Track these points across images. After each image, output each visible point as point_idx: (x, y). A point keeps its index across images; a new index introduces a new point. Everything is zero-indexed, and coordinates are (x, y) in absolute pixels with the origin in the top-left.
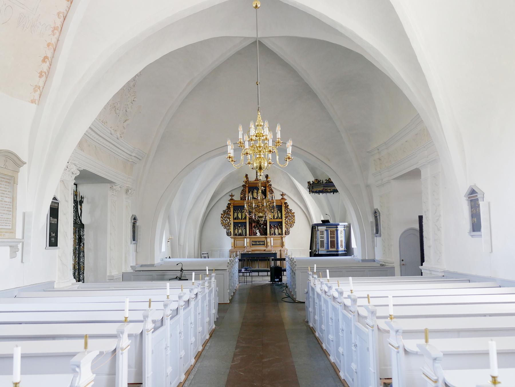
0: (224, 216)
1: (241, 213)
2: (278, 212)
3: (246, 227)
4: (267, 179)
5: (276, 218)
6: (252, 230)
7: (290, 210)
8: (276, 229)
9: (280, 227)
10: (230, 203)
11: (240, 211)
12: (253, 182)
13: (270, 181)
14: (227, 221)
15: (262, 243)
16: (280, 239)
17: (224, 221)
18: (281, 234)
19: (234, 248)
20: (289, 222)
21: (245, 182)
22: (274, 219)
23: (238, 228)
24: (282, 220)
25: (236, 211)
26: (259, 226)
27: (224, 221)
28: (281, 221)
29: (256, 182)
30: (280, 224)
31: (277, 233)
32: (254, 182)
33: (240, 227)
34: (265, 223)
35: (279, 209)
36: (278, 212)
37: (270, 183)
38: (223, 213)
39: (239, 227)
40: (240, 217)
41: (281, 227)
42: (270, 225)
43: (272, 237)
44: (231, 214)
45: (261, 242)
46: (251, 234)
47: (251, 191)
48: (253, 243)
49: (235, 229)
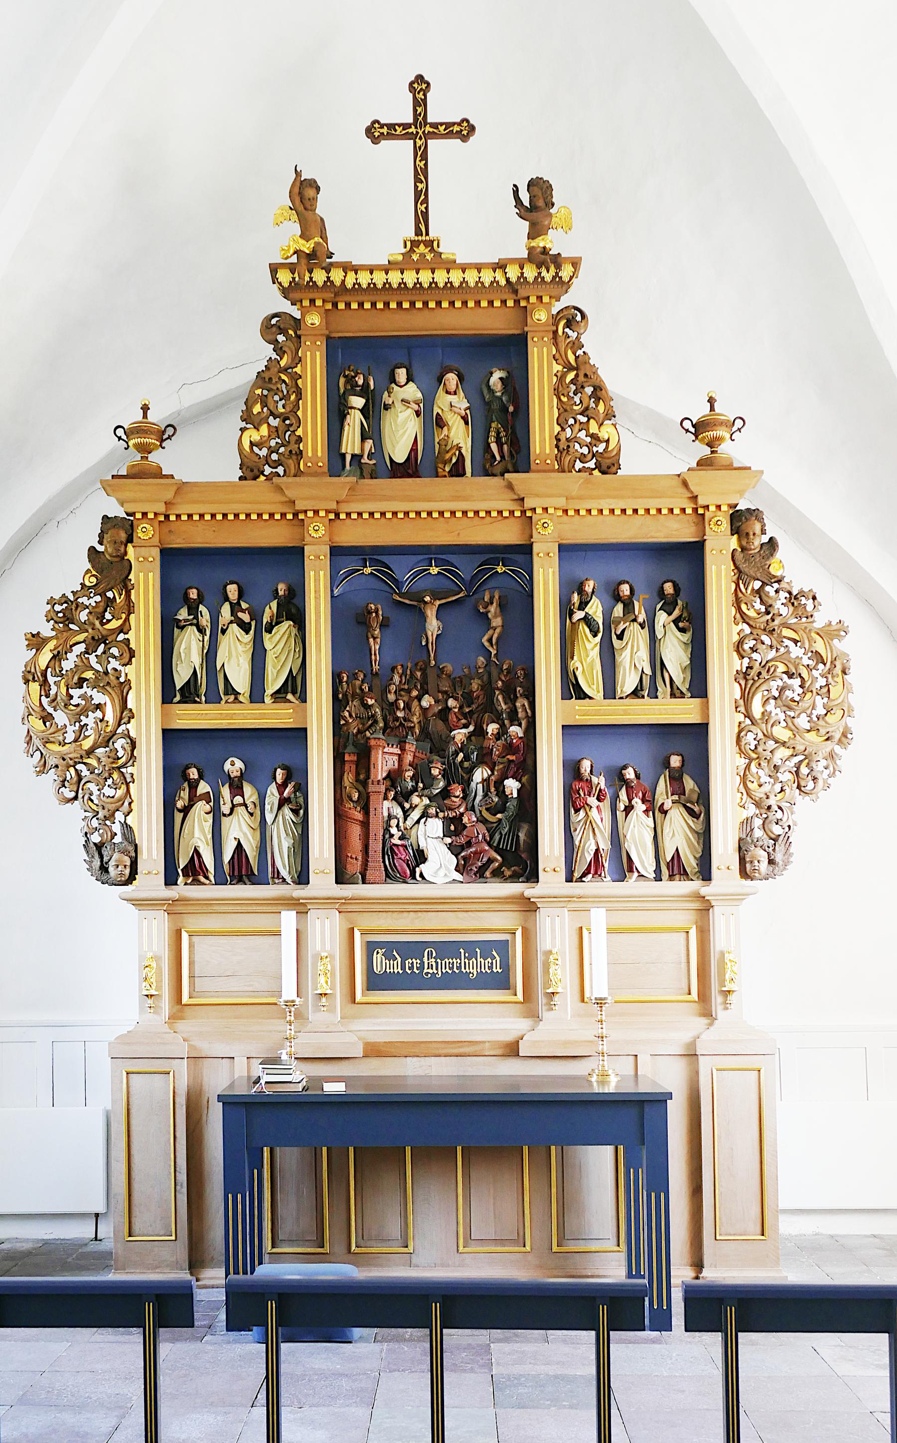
0: (57, 657)
1: (245, 627)
2: (662, 618)
3: (302, 788)
4: (535, 232)
5: (636, 693)
6: (365, 825)
7: (793, 599)
8: (629, 809)
9: (677, 788)
10: (117, 511)
11: (235, 608)
12: (379, 278)
13: (576, 263)
14: (90, 720)
15: (474, 967)
16: (685, 918)
17: (61, 718)
18: (690, 861)
19: (174, 1017)
20: (781, 733)
21: (285, 277)
22: (610, 692)
23: (218, 796)
24: (705, 709)
25: (193, 610)
26: (445, 774)
27: (61, 718)
28: (693, 718)
29: (410, 278)
30: (675, 761)
31: (644, 861)
32: (395, 278)
33: (236, 789)
34: (510, 748)
35: (669, 588)
36: (662, 618)
37: (566, 301)
38: (46, 630)
39: (226, 791)
40: (240, 679)
41: (689, 784)
42: (572, 771)
43: (599, 900)
44: (131, 636)
45: (470, 947)
46: (354, 867)
47: (364, 392)
48: (377, 969)
49: (186, 810)
